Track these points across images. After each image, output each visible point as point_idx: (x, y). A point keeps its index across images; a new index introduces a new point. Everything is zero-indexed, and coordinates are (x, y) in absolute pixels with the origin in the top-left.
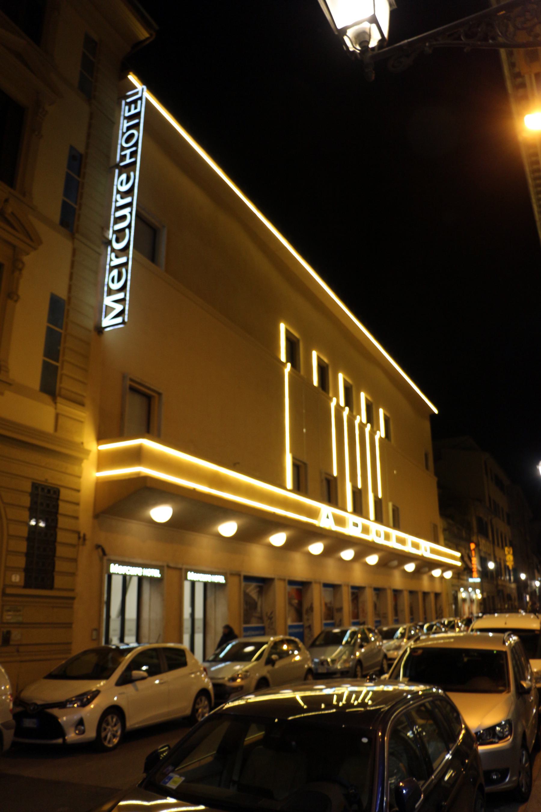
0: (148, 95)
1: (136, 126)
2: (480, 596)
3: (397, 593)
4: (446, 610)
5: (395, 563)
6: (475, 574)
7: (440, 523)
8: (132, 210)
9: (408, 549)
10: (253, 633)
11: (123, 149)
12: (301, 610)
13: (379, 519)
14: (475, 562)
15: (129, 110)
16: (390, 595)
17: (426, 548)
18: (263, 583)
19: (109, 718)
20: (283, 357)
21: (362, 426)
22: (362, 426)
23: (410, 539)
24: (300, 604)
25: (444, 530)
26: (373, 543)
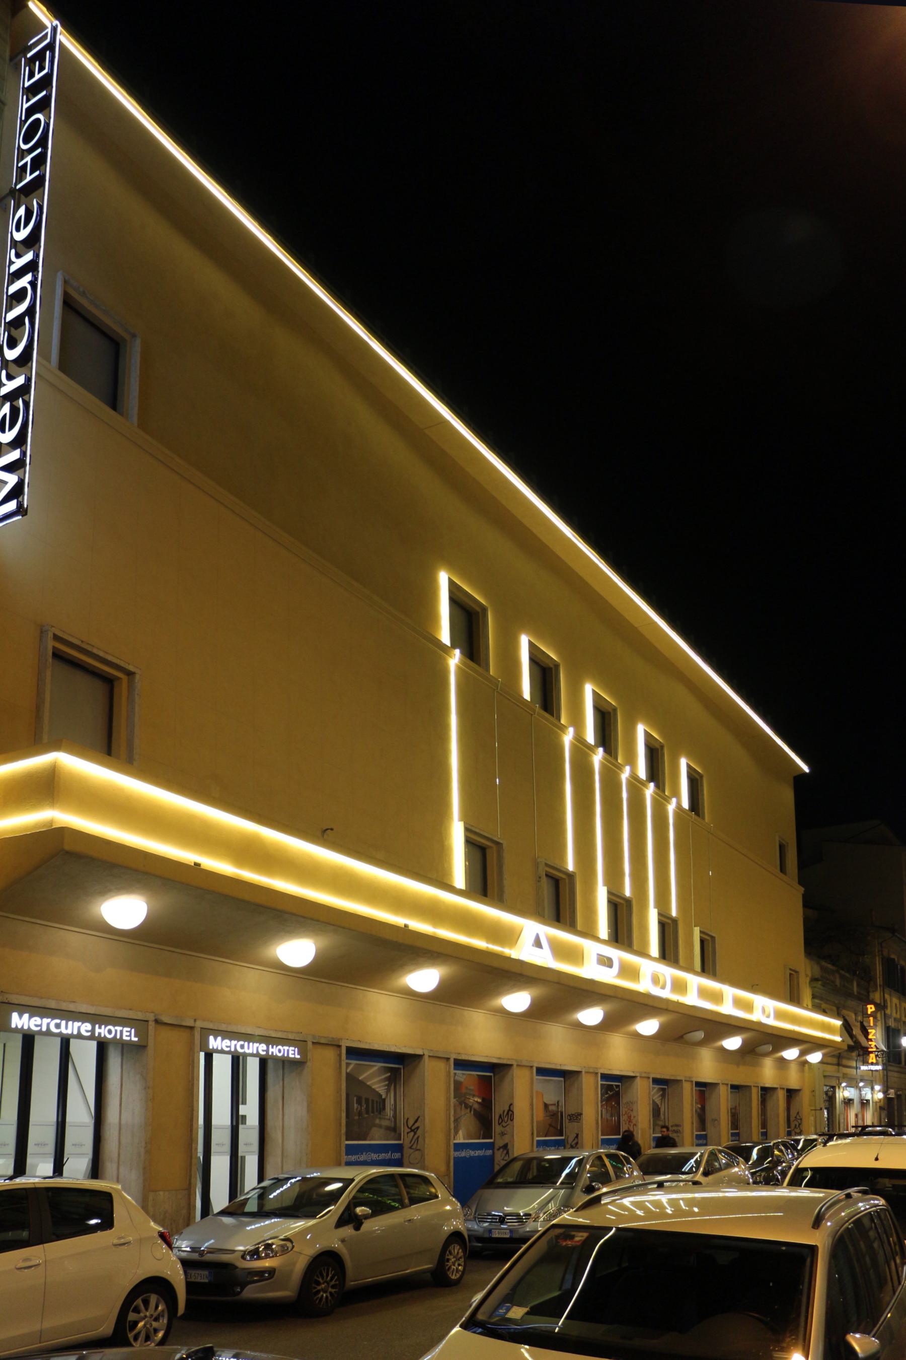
0: (65, 39)
1: (42, 106)
2: (880, 1096)
3: (704, 1089)
4: (809, 1121)
5: (700, 1035)
6: (872, 1058)
7: (805, 968)
8: (35, 278)
9: (727, 1008)
10: (374, 1156)
11: (22, 154)
12: (487, 1116)
13: (668, 954)
14: (876, 1037)
15: (31, 75)
16: (688, 1094)
17: (765, 1010)
18: (400, 1064)
19: (451, 1248)
20: (445, 636)
21: (636, 786)
22: (636, 786)
23: (729, 992)
24: (487, 1104)
25: (814, 980)
26: (648, 996)
